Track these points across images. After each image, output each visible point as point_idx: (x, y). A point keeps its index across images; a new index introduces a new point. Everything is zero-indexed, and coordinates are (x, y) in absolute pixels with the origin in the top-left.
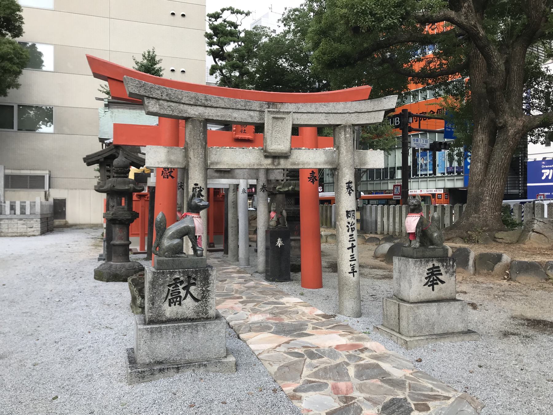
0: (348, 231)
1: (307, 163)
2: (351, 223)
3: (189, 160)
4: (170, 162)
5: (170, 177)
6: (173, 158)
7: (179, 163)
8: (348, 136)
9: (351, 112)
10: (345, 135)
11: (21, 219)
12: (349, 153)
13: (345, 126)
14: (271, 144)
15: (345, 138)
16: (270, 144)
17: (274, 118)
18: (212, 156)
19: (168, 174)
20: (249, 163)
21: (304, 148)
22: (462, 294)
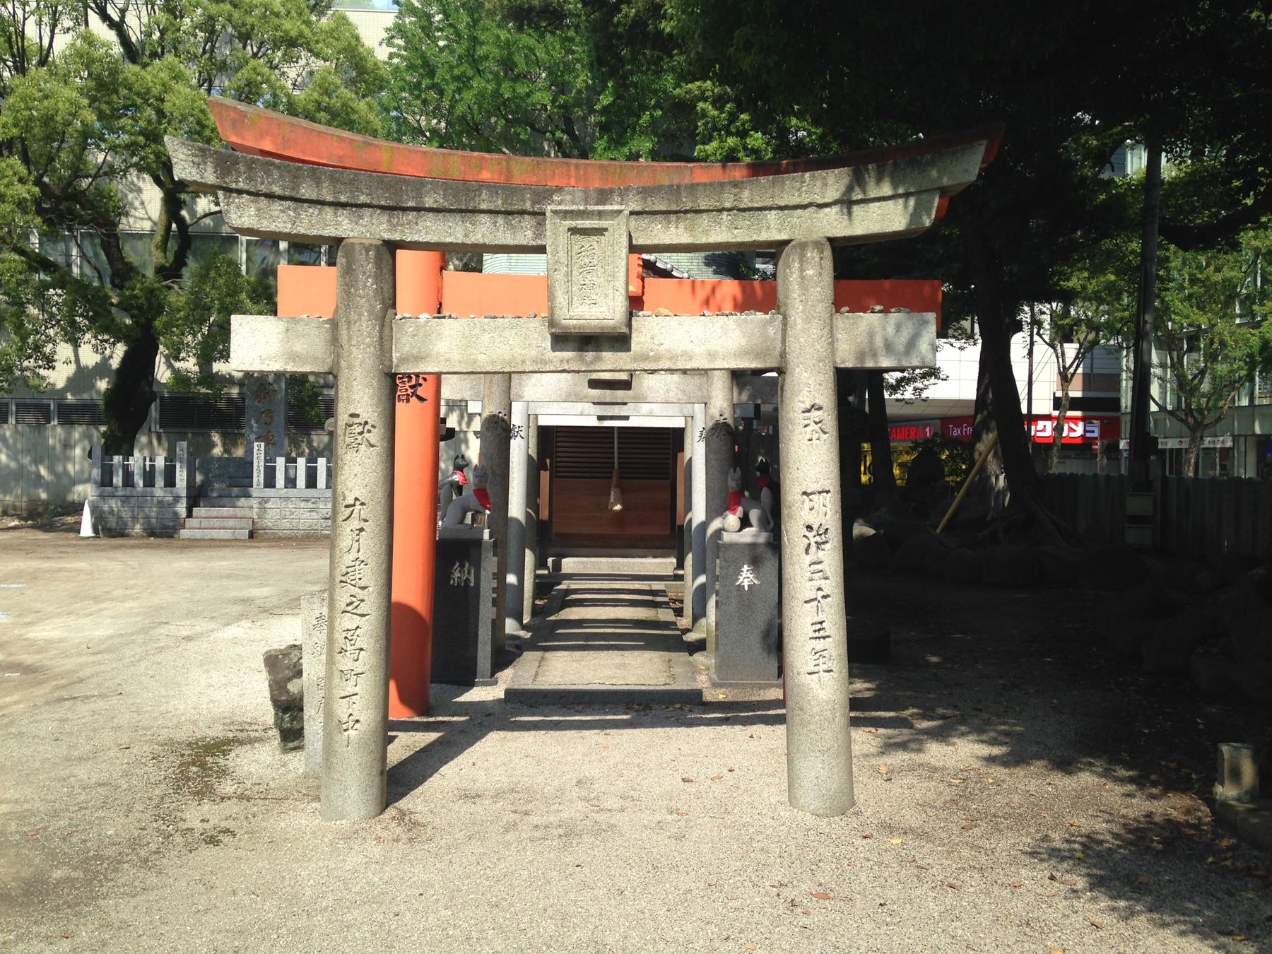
0: (807, 551)
1: (684, 354)
2: (815, 527)
3: (340, 351)
4: (293, 357)
5: (413, 399)
6: (299, 347)
7: (316, 359)
8: (810, 272)
9: (820, 201)
10: (802, 270)
11: (307, 500)
12: (815, 322)
13: (803, 246)
14: (571, 303)
15: (803, 278)
16: (565, 303)
17: (574, 231)
18: (404, 340)
19: (410, 391)
20: (507, 357)
21: (878, 308)
22: (78, 686)
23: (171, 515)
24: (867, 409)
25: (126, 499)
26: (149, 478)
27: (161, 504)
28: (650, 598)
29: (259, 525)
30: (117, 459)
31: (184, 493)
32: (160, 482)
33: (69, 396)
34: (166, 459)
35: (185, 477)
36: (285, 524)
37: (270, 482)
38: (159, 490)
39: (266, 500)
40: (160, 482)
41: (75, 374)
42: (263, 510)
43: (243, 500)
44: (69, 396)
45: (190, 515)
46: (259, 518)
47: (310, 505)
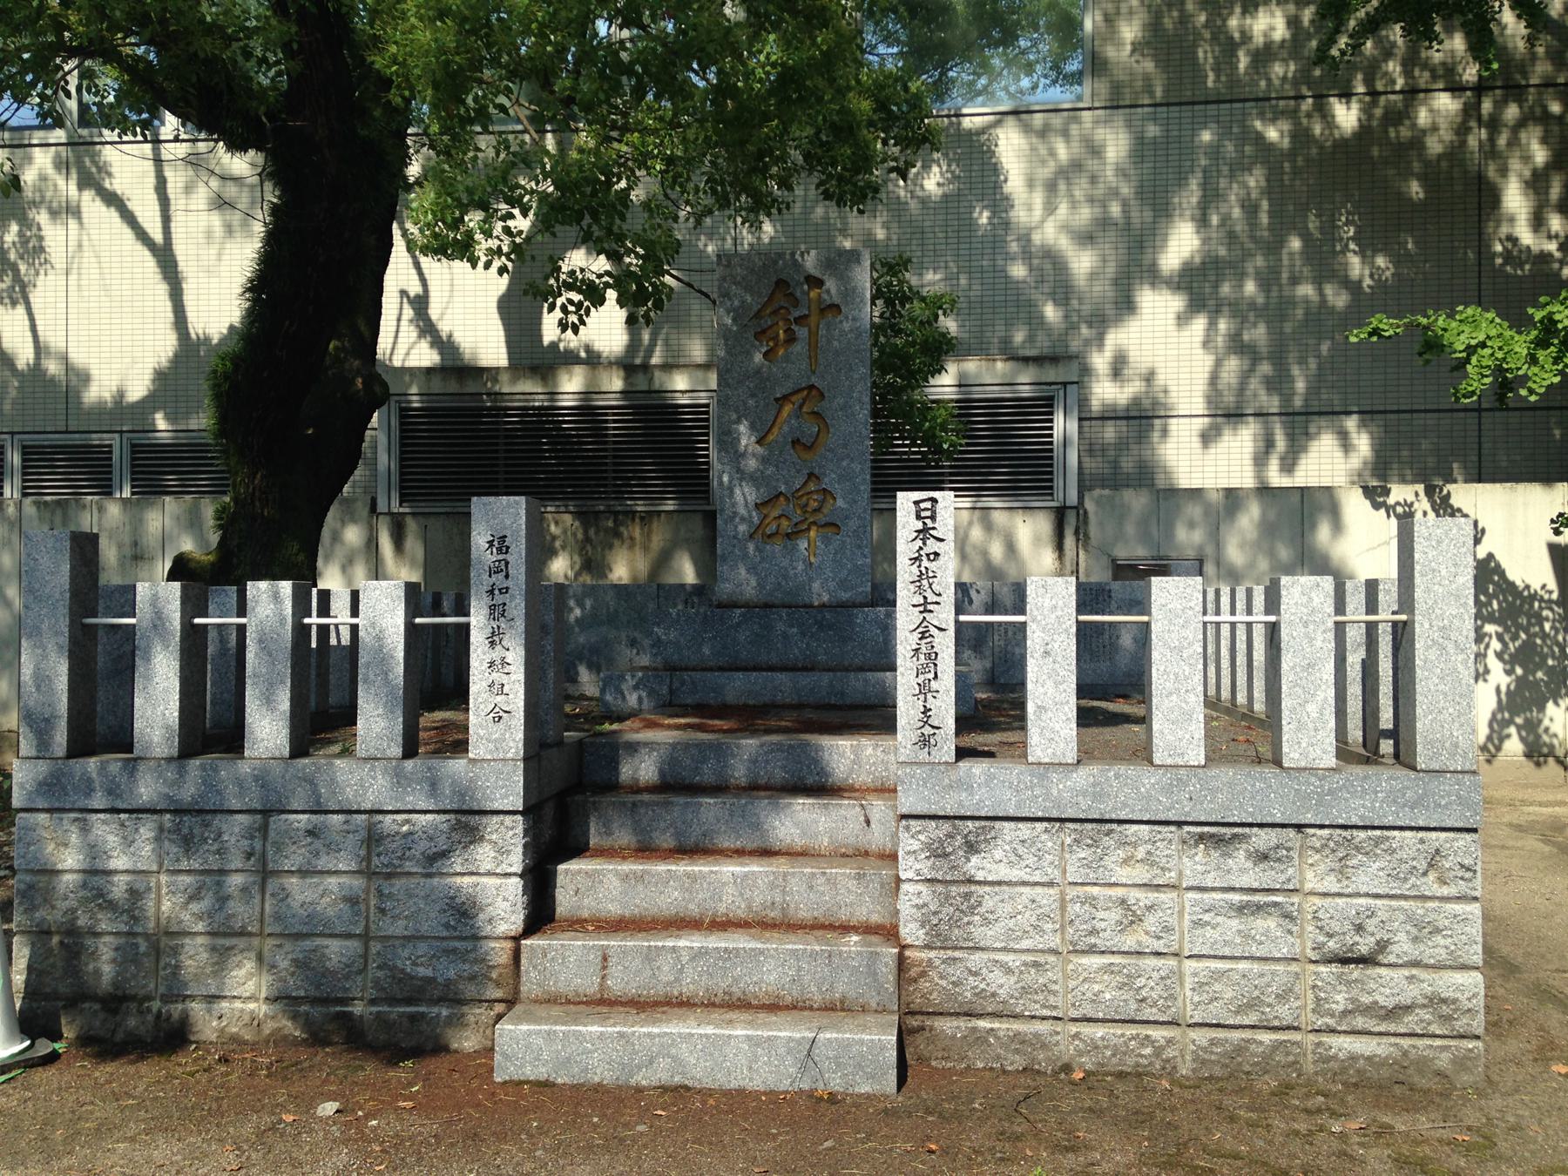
11: (1218, 835)
23: (431, 922)
24: (314, 645)
25: (187, 823)
26: (322, 719)
27: (375, 847)
28: (1245, 898)
29: (933, 988)
30: (269, 601)
31: (507, 790)
32: (376, 722)
33: (161, 423)
34: (414, 598)
35: (516, 699)
36: (1092, 982)
37: (991, 708)
38: (369, 763)
39: (969, 830)
40: (376, 722)
41: (177, 359)
42: (958, 889)
43: (802, 807)
44: (161, 423)
45: (540, 912)
46: (938, 939)
47: (1241, 869)
